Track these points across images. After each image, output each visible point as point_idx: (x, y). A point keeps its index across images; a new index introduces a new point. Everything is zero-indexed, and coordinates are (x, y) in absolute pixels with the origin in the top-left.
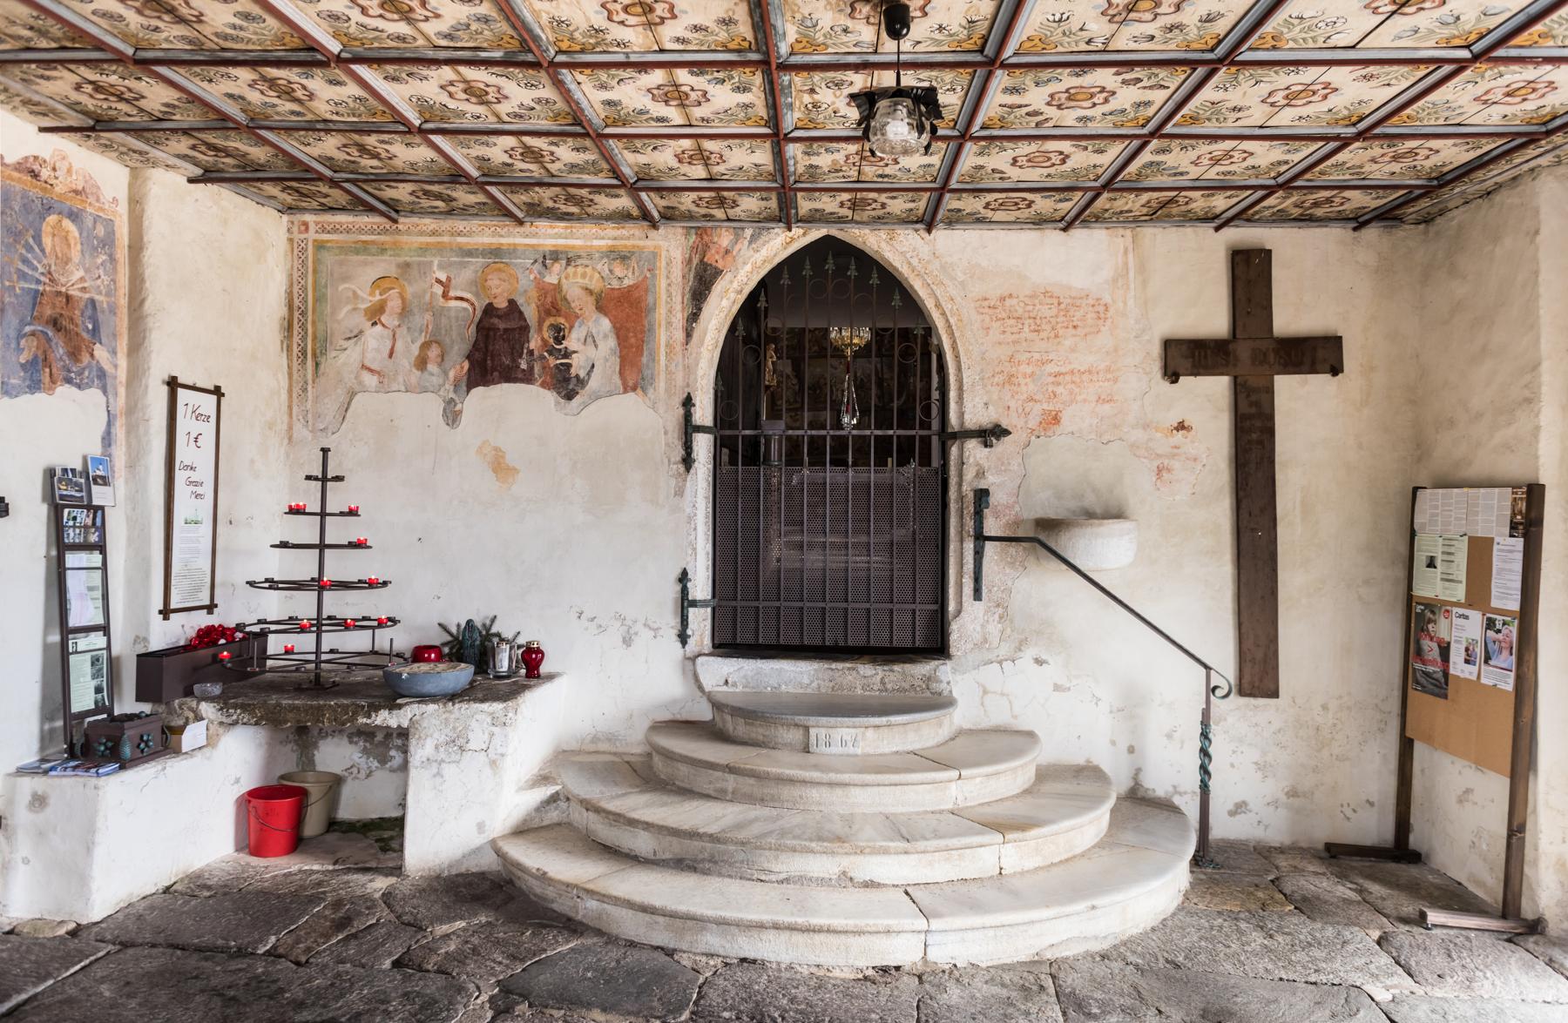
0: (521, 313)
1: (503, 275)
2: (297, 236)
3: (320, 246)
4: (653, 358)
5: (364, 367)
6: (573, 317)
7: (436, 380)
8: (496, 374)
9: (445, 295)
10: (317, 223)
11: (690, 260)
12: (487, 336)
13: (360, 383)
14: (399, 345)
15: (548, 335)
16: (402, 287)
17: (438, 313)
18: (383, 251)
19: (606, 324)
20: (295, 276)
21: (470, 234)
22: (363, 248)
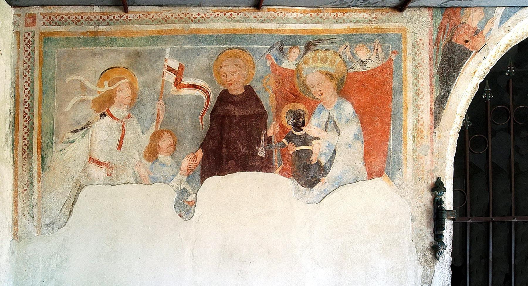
0: (258, 100)
1: (240, 62)
2: (23, 29)
3: (46, 38)
4: (401, 137)
5: (92, 160)
6: (313, 104)
7: (168, 171)
8: (231, 162)
9: (177, 84)
10: (44, 16)
11: (437, 42)
12: (222, 124)
13: (87, 176)
14: (128, 135)
15: (287, 121)
16: (132, 77)
17: (169, 101)
18: (112, 41)
19: (348, 108)
20: (22, 68)
21: (204, 20)
22: (94, 38)
